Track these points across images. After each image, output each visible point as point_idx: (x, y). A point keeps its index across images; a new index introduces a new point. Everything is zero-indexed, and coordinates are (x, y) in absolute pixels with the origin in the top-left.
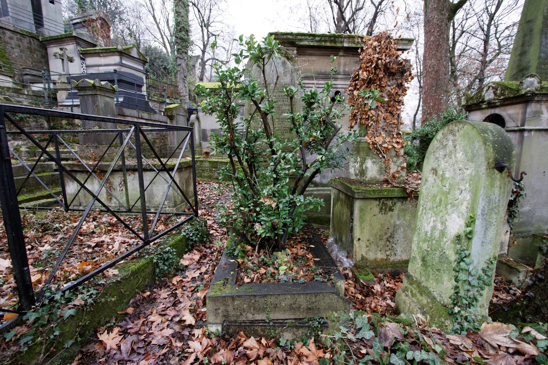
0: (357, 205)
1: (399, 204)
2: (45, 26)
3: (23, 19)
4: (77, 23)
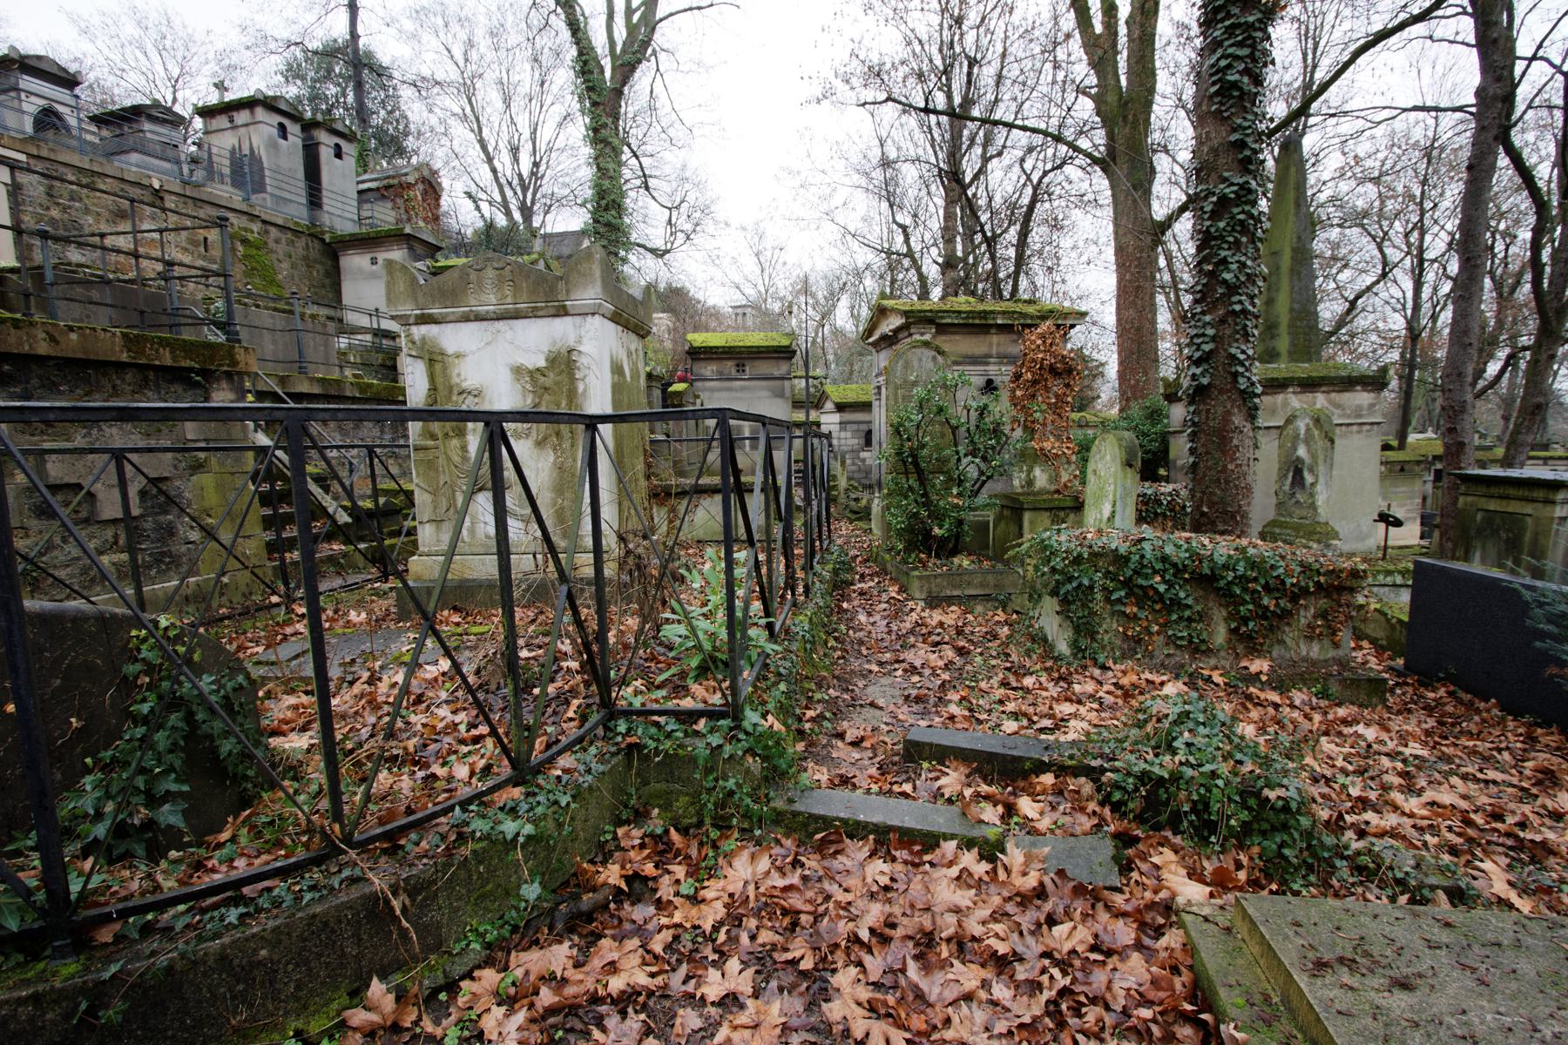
0: (1027, 516)
1: (1072, 516)
2: (326, 208)
3: (288, 196)
4: (370, 190)
